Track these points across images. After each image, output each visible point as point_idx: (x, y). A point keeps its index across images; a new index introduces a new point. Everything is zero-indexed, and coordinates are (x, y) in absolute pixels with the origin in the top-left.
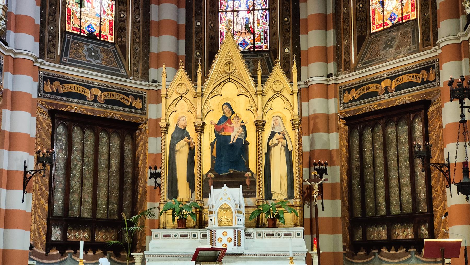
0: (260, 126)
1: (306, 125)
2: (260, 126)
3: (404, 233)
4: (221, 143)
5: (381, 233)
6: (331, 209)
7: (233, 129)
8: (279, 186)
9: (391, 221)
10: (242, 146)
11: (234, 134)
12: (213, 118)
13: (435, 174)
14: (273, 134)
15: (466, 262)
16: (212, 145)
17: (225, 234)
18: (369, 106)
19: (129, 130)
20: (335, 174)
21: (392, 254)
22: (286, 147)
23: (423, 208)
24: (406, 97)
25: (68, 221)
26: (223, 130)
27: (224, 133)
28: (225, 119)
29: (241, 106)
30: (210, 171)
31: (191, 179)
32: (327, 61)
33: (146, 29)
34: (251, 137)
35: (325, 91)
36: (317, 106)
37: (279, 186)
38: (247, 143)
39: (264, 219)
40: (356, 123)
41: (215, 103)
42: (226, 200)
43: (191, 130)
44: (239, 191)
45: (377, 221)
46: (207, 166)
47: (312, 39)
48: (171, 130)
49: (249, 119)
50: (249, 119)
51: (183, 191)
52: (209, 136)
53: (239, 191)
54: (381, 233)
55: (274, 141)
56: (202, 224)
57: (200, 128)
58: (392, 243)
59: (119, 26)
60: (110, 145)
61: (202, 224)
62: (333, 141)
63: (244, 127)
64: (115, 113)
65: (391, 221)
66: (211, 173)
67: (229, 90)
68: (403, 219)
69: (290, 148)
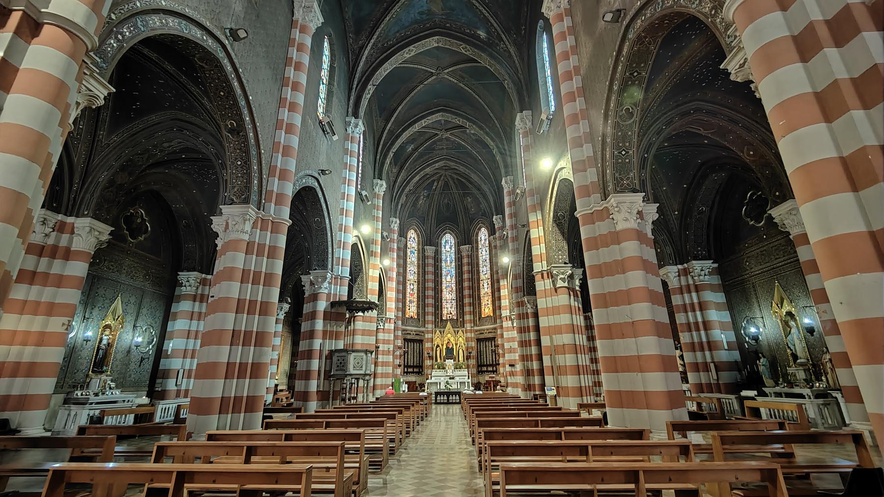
0: (456, 344)
1: (467, 340)
2: (456, 344)
3: (490, 369)
4: (447, 348)
5: (485, 369)
6: (473, 362)
8: (461, 359)
9: (487, 366)
12: (445, 342)
15: (293, 2)
18: (482, 336)
19: (421, 342)
20: (474, 353)
24: (490, 335)
25: (408, 367)
29: (452, 339)
33: (424, 314)
35: (471, 331)
36: (469, 335)
37: (461, 359)
39: (457, 367)
40: (479, 340)
42: (450, 363)
45: (484, 366)
47: (467, 317)
50: (454, 342)
51: (439, 360)
52: (445, 347)
54: (485, 369)
56: (444, 368)
58: (487, 371)
59: (418, 315)
60: (417, 345)
61: (444, 368)
62: (473, 344)
64: (418, 338)
65: (487, 366)
66: (242, 37)
67: (449, 335)
68: (490, 365)
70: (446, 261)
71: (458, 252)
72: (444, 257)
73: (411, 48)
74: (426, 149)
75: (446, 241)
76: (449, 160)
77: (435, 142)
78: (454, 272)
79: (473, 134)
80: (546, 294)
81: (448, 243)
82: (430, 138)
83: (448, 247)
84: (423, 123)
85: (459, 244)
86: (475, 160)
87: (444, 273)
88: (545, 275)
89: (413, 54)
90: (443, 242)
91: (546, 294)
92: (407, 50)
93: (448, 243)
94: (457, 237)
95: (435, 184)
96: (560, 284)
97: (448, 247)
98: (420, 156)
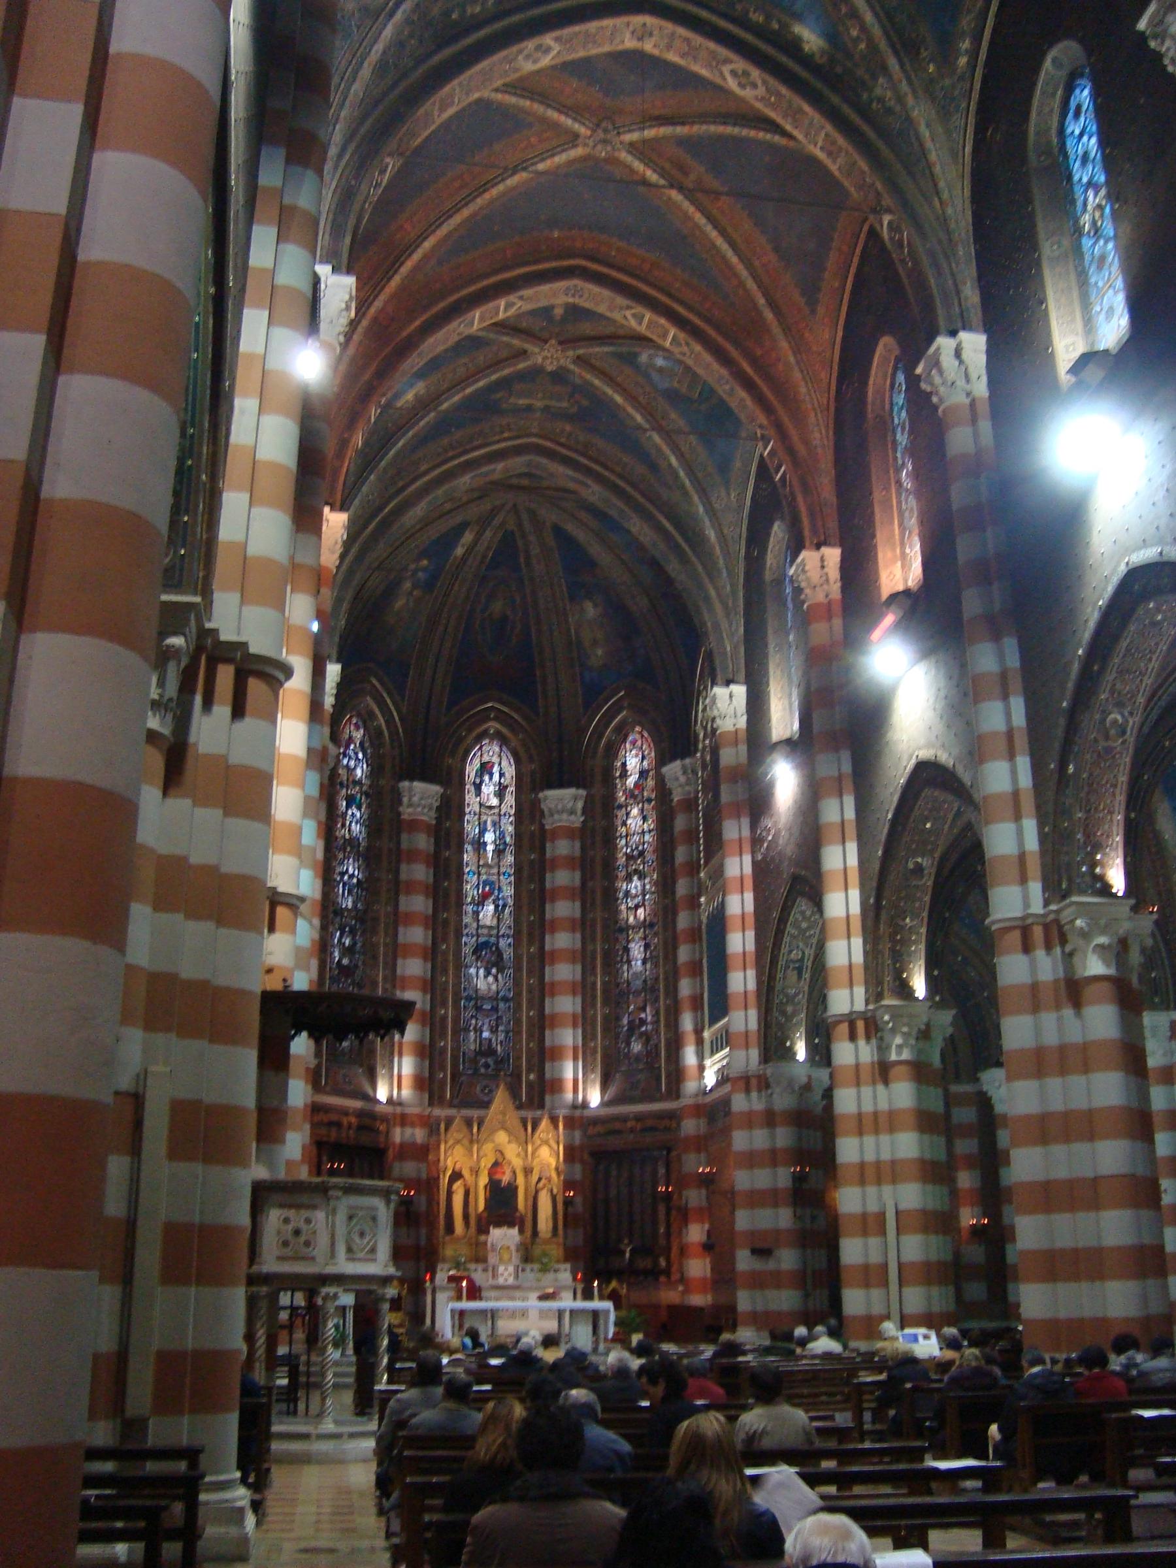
2: (528, 1171)
7: (504, 1173)
10: (512, 1189)
11: (506, 1179)
12: (486, 1163)
13: (674, 1212)
14: (540, 1179)
16: (486, 1187)
17: (506, 1269)
21: (930, 980)
22: (552, 1191)
23: (662, 1241)
26: (495, 1173)
27: (497, 1177)
28: (496, 1164)
29: (513, 1153)
30: (293, 1037)
31: (466, 1216)
32: (574, 869)
34: (520, 1181)
38: (516, 1188)
41: (488, 1148)
43: (466, 1173)
44: (515, 1231)
46: (481, 1206)
48: (449, 1173)
49: (517, 1163)
50: (517, 1163)
52: (483, 1180)
53: (515, 1231)
55: (541, 1185)
57: (476, 1172)
63: (514, 1173)
69: (555, 1191)
70: (480, 845)
71: (528, 812)
72: (471, 828)
73: (548, 39)
74: (467, 404)
75: (486, 768)
76: (551, 455)
77: (504, 384)
78: (508, 891)
79: (661, 370)
80: (1034, 998)
81: (491, 781)
82: (497, 364)
83: (488, 789)
84: (504, 308)
85: (530, 786)
86: (653, 467)
87: (471, 889)
88: (1038, 933)
89: (546, 61)
90: (471, 770)
91: (1034, 998)
92: (740, 64)
93: (491, 781)
94: (657, 742)
95: (468, 537)
96: (1095, 966)
97: (488, 789)
98: (442, 427)
